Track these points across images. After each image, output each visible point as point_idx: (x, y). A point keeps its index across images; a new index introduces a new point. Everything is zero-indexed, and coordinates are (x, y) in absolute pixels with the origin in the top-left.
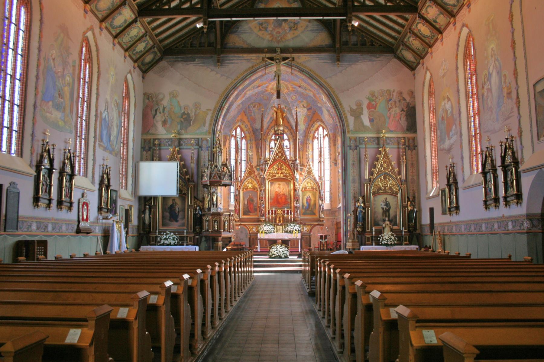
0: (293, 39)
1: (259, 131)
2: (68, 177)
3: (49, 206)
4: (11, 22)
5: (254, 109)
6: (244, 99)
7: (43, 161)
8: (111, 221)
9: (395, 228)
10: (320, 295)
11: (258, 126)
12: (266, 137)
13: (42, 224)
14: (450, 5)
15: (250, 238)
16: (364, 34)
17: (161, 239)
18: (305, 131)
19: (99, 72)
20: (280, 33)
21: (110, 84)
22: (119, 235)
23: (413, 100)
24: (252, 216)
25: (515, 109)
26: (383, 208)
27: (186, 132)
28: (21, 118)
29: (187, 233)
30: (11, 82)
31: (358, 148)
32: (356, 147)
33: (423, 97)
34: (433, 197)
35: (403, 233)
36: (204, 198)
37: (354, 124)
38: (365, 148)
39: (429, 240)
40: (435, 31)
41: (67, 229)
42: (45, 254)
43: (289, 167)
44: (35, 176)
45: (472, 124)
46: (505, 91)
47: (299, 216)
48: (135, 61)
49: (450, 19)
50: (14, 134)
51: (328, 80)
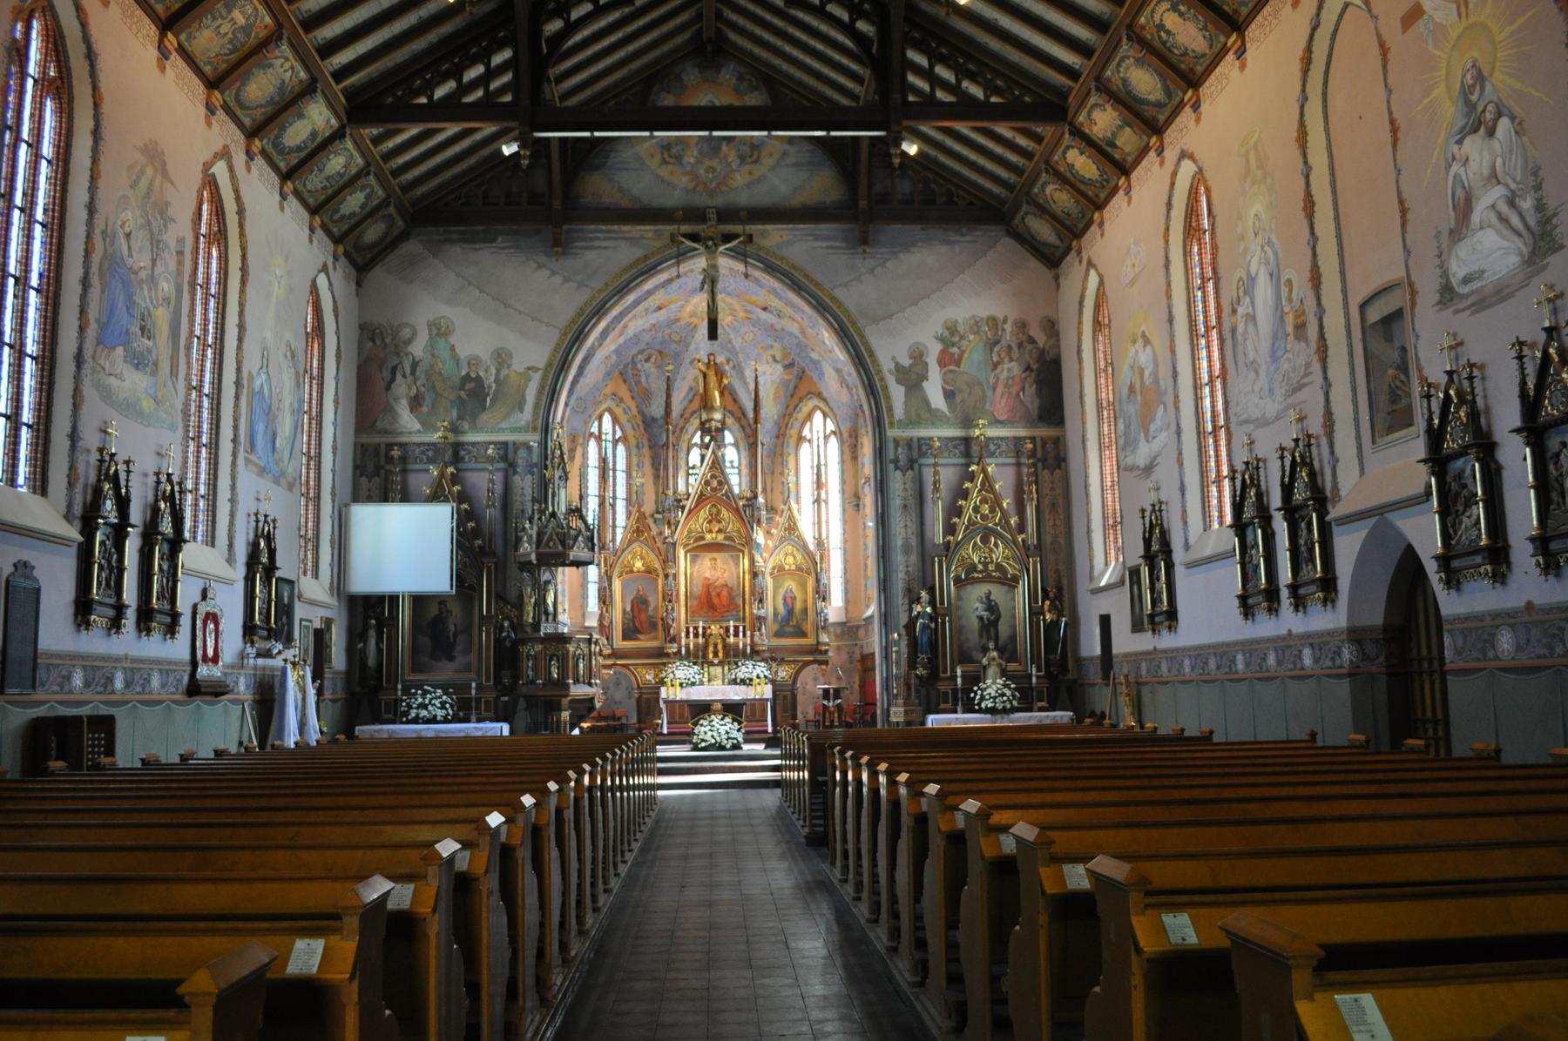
0: (749, 185)
1: (661, 422)
2: (166, 547)
3: (115, 624)
4: (17, 139)
5: (647, 365)
6: (621, 341)
7: (98, 501)
8: (277, 662)
9: (1013, 666)
10: (845, 841)
11: (657, 410)
12: (679, 438)
13: (99, 672)
14: (1148, 103)
15: (639, 700)
16: (929, 175)
17: (410, 707)
18: (777, 423)
19: (244, 269)
20: (714, 169)
21: (274, 299)
22: (299, 696)
23: (1052, 342)
24: (645, 643)
25: (1316, 367)
26: (981, 618)
27: (475, 428)
28: (41, 390)
29: (479, 687)
30: (15, 296)
31: (916, 466)
32: (912, 463)
33: (1080, 334)
34: (1108, 587)
35: (1034, 680)
36: (521, 597)
37: (906, 403)
38: (935, 465)
39: (1101, 698)
40: (1110, 168)
41: (163, 686)
42: (110, 751)
43: (741, 514)
44: (80, 545)
45: (1207, 402)
46: (1290, 321)
47: (765, 640)
48: (337, 240)
49: (1150, 138)
50: (25, 434)
51: (839, 293)
